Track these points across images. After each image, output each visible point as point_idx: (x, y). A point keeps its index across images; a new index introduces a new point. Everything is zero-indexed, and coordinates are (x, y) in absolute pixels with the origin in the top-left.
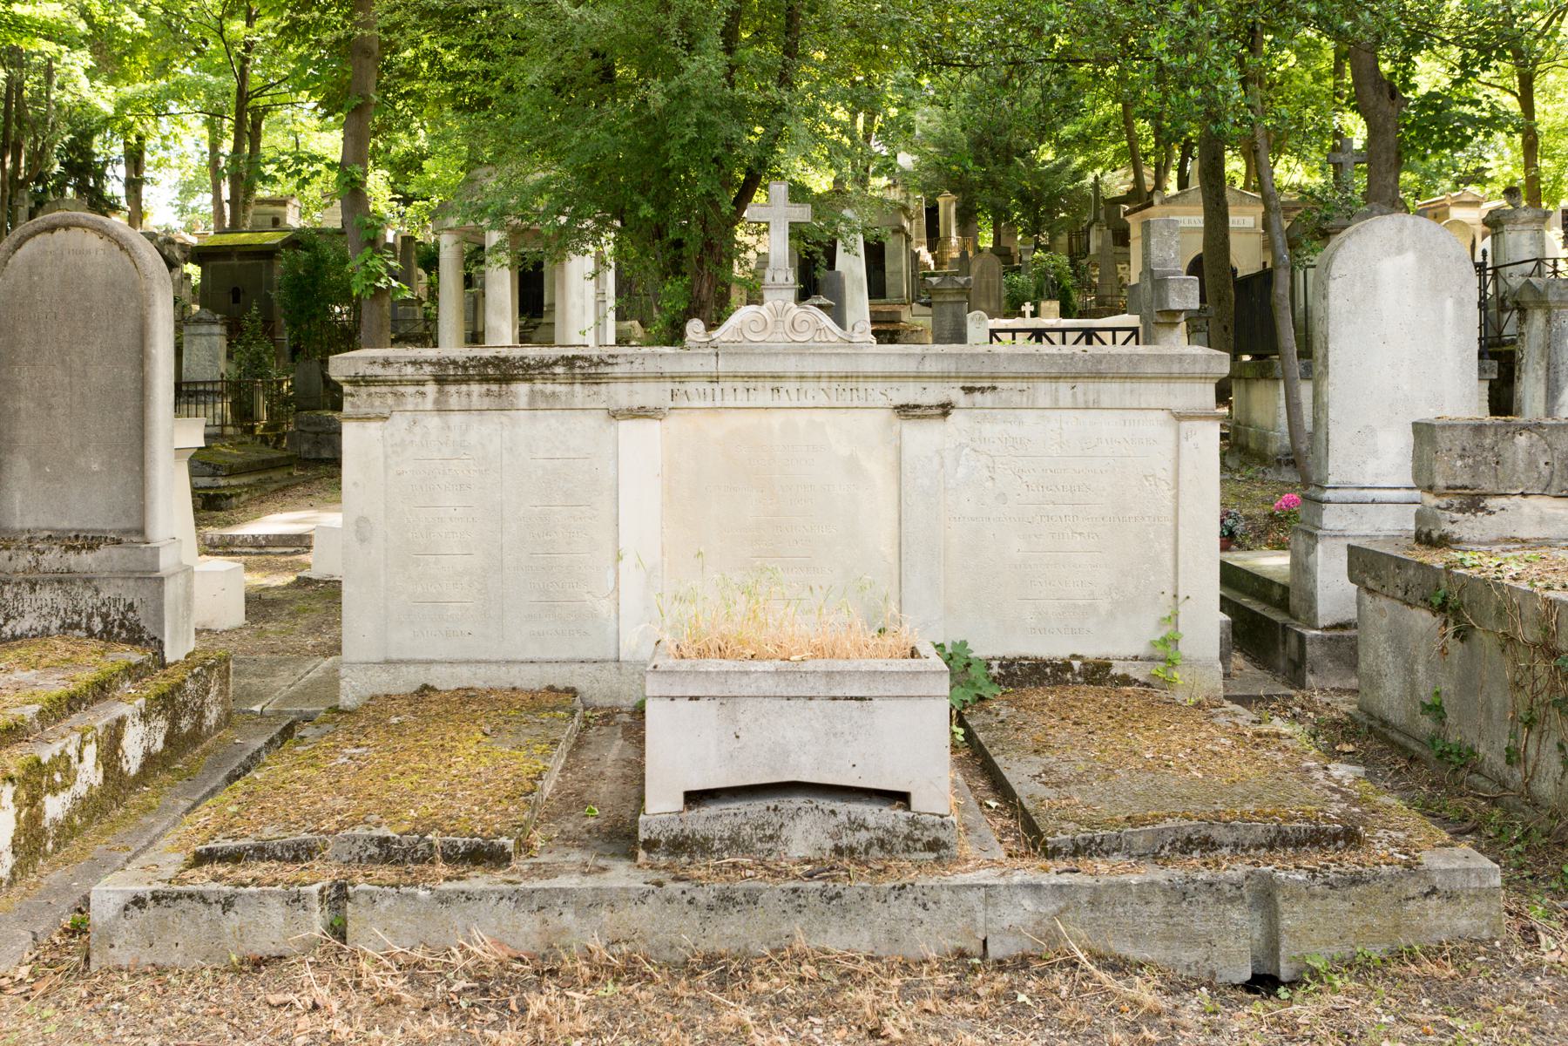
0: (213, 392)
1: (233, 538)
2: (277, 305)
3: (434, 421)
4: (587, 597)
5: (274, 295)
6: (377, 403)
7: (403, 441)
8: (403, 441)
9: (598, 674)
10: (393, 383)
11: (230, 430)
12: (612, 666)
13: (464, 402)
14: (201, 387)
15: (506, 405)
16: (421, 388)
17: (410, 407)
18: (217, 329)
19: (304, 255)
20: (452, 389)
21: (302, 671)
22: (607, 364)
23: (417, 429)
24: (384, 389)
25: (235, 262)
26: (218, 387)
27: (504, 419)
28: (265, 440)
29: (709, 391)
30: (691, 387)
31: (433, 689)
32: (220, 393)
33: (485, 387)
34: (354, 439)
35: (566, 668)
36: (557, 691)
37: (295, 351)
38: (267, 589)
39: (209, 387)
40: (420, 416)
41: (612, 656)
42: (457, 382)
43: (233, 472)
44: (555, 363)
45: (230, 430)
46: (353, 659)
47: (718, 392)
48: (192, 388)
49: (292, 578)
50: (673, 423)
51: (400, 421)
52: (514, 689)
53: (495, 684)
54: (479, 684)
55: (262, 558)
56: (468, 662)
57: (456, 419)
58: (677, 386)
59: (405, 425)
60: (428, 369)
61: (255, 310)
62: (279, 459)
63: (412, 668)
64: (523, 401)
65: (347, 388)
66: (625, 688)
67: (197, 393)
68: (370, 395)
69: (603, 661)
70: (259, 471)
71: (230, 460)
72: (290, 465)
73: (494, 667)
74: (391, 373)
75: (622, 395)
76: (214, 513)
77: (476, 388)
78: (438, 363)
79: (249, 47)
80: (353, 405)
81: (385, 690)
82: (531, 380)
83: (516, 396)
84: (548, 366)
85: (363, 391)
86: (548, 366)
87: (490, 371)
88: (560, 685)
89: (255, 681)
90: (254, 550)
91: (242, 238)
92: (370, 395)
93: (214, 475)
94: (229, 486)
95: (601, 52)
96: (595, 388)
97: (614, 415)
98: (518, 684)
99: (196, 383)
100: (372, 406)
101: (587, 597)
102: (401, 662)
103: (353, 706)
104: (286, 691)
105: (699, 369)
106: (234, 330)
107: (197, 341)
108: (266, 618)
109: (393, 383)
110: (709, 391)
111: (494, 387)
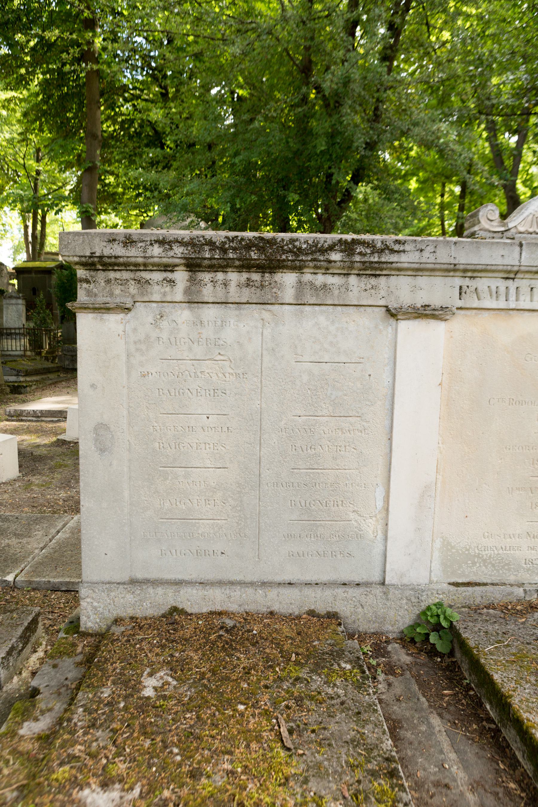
0: (19, 334)
1: (22, 411)
2: (53, 296)
3: (184, 315)
4: (352, 516)
5: (52, 291)
6: (117, 292)
7: (148, 337)
8: (148, 337)
9: (363, 599)
10: (136, 267)
11: (28, 353)
12: (378, 591)
13: (220, 295)
14: (13, 331)
15: (268, 297)
16: (169, 275)
17: (156, 297)
18: (20, 301)
19: (65, 272)
20: (206, 277)
21: (53, 531)
22: (392, 251)
23: (164, 324)
24: (126, 275)
25: (33, 275)
26: (22, 331)
27: (266, 315)
28: (47, 359)
29: (502, 289)
30: (483, 283)
31: (182, 612)
32: (23, 334)
33: (245, 275)
34: (91, 332)
35: (328, 593)
36: (319, 616)
37: (63, 318)
38: (38, 446)
39: (17, 331)
40: (168, 308)
41: (376, 577)
42: (213, 268)
43: (28, 374)
44: (331, 248)
45: (28, 353)
46: (95, 579)
47: (512, 291)
48: (9, 331)
49: (54, 439)
50: (458, 325)
51: (144, 314)
52: (271, 613)
53: (251, 608)
54: (233, 607)
55: (38, 424)
56: (220, 583)
57: (210, 313)
58: (467, 282)
59: (150, 319)
60: (178, 250)
61: (42, 296)
62: (53, 368)
63: (160, 590)
64: (289, 295)
65: (81, 273)
66: (392, 613)
67: (11, 334)
68: (108, 281)
69: (367, 584)
70: (42, 374)
71: (26, 367)
72: (58, 371)
73: (250, 591)
74: (134, 253)
75: (403, 290)
76: (16, 395)
77: (234, 277)
78: (191, 243)
79: (38, 173)
80: (89, 293)
81: (130, 612)
82: (299, 269)
83: (281, 286)
84: (323, 251)
85: (101, 276)
86: (323, 251)
87: (254, 255)
88: (321, 609)
89: (14, 541)
90: (34, 419)
91: (37, 264)
92: (108, 281)
93: (17, 375)
94: (26, 381)
95: (145, 286)
96: (373, 281)
97: (392, 314)
98: (276, 608)
99: (11, 329)
100: (111, 294)
101: (352, 516)
102: (146, 582)
103: (96, 628)
104: (39, 555)
105: (499, 261)
106: (30, 306)
107: (10, 307)
108: (33, 471)
109: (136, 267)
110: (502, 289)
111: (256, 277)
